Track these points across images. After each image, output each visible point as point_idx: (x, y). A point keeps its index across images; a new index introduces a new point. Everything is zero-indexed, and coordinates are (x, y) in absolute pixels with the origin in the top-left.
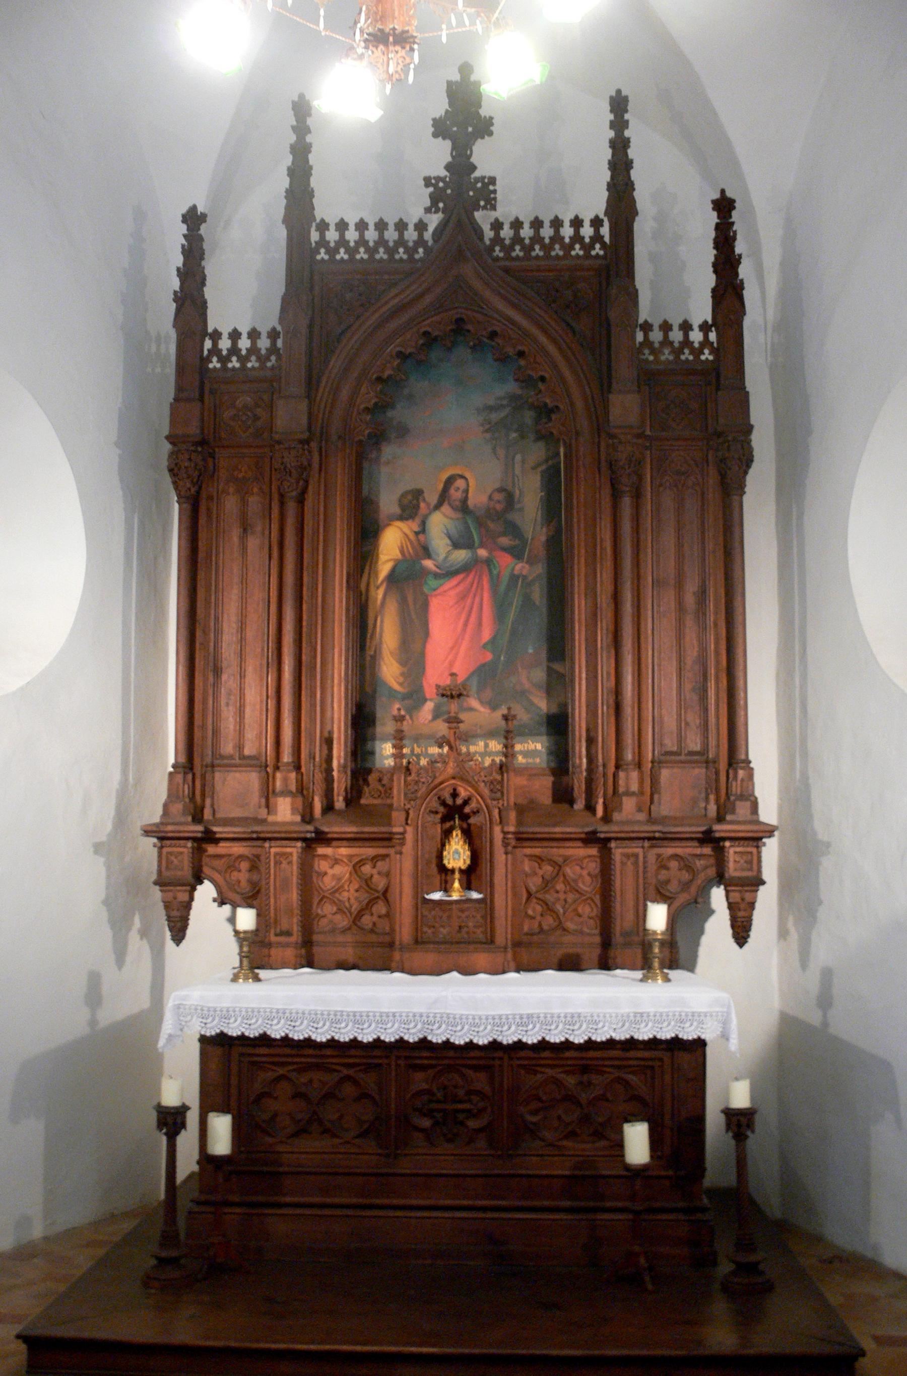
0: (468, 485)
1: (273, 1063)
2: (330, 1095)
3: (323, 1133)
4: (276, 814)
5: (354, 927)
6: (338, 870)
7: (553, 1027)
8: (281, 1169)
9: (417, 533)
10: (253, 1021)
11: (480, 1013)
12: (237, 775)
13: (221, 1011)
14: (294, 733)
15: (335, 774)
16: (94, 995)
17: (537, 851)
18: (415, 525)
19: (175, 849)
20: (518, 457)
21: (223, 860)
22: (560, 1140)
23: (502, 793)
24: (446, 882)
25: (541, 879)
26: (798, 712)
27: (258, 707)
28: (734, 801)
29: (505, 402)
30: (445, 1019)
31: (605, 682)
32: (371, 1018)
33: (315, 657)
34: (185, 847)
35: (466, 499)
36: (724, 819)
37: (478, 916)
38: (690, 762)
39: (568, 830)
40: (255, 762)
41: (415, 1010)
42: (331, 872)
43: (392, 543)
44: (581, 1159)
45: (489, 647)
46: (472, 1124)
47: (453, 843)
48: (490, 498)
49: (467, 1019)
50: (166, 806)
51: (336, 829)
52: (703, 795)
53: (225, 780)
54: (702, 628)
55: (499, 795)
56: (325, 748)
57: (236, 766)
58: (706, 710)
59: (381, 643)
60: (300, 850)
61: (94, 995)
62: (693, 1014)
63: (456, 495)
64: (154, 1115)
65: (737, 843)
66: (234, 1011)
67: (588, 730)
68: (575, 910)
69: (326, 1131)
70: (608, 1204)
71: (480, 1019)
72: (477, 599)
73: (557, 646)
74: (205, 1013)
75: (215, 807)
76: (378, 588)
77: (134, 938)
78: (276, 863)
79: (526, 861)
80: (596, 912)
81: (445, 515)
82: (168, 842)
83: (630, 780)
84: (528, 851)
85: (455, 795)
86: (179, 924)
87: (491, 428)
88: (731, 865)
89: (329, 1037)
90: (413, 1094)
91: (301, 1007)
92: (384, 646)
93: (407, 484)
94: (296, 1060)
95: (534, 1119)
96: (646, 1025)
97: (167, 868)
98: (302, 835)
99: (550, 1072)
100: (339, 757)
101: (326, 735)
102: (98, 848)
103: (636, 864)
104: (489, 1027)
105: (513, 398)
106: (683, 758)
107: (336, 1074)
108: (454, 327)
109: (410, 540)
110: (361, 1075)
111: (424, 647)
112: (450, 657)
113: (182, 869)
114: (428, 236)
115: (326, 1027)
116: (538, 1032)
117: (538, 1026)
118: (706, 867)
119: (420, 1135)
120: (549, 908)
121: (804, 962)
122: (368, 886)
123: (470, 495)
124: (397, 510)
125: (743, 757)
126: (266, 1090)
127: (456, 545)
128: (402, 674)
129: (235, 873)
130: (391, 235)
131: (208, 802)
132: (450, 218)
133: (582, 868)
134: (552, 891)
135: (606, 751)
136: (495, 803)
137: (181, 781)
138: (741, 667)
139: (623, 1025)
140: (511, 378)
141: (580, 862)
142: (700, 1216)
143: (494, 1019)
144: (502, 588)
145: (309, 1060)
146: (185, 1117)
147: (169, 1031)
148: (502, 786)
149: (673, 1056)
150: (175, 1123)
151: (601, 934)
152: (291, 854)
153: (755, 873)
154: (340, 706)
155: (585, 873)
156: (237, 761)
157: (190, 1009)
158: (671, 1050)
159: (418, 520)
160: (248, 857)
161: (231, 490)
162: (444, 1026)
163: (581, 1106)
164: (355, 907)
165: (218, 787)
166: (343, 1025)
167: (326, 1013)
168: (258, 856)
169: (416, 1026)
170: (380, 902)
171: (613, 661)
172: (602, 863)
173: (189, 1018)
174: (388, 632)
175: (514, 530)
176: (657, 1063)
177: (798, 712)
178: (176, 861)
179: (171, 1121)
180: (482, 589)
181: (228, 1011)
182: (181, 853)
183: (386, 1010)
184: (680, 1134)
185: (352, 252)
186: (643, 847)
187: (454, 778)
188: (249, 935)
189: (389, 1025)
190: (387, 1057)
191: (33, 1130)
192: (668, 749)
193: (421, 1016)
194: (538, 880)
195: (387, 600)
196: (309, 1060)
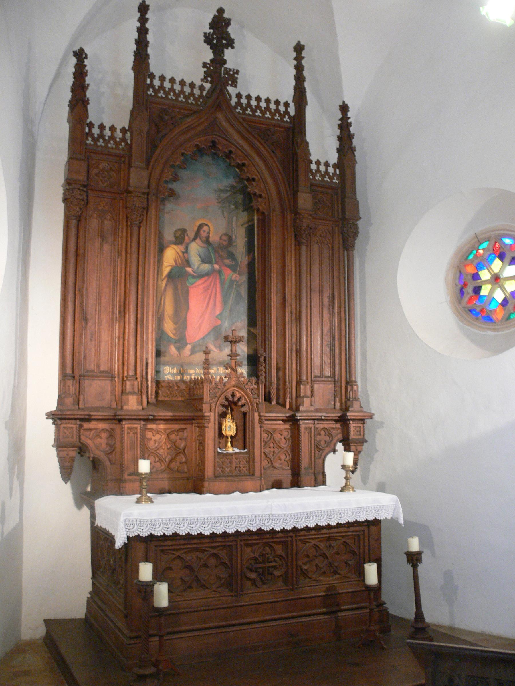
0: (210, 230)
1: (174, 550)
4: (128, 405)
6: (157, 437)
7: (322, 518)
8: (180, 611)
9: (183, 253)
10: (170, 526)
12: (99, 382)
18: (182, 248)
20: (234, 218)
21: (93, 432)
28: (352, 401)
29: (228, 189)
32: (302, 516)
34: (76, 424)
35: (208, 237)
36: (299, 410)
40: (107, 375)
41: (256, 513)
43: (170, 255)
44: (328, 586)
45: (219, 317)
46: (276, 573)
48: (221, 238)
51: (161, 414)
52: (333, 398)
54: (332, 314)
57: (96, 376)
58: (334, 356)
59: (163, 311)
62: (383, 506)
63: (204, 234)
66: (158, 521)
67: (277, 364)
68: (279, 457)
71: (288, 516)
72: (214, 291)
81: (197, 244)
85: (233, 396)
87: (221, 201)
89: (211, 532)
91: (195, 516)
92: (166, 313)
93: (178, 225)
94: (187, 546)
95: (305, 567)
99: (313, 542)
105: (232, 187)
107: (206, 553)
108: (211, 145)
109: (180, 256)
110: (221, 552)
111: (187, 314)
112: (200, 322)
113: (72, 437)
114: (204, 93)
115: (210, 526)
123: (211, 235)
124: (174, 239)
127: (203, 261)
128: (175, 329)
129: (99, 440)
130: (177, 87)
132: (215, 88)
135: (291, 377)
136: (255, 400)
138: (353, 335)
140: (231, 177)
145: (193, 546)
151: (291, 469)
152: (137, 428)
159: (184, 246)
160: (108, 430)
161: (95, 215)
163: (327, 558)
166: (219, 524)
167: (209, 518)
168: (113, 430)
170: (181, 454)
172: (343, 433)
175: (231, 256)
181: (155, 521)
182: (72, 428)
183: (241, 514)
185: (167, 93)
187: (234, 387)
188: (147, 476)
189: (243, 523)
193: (259, 516)
196: (193, 546)
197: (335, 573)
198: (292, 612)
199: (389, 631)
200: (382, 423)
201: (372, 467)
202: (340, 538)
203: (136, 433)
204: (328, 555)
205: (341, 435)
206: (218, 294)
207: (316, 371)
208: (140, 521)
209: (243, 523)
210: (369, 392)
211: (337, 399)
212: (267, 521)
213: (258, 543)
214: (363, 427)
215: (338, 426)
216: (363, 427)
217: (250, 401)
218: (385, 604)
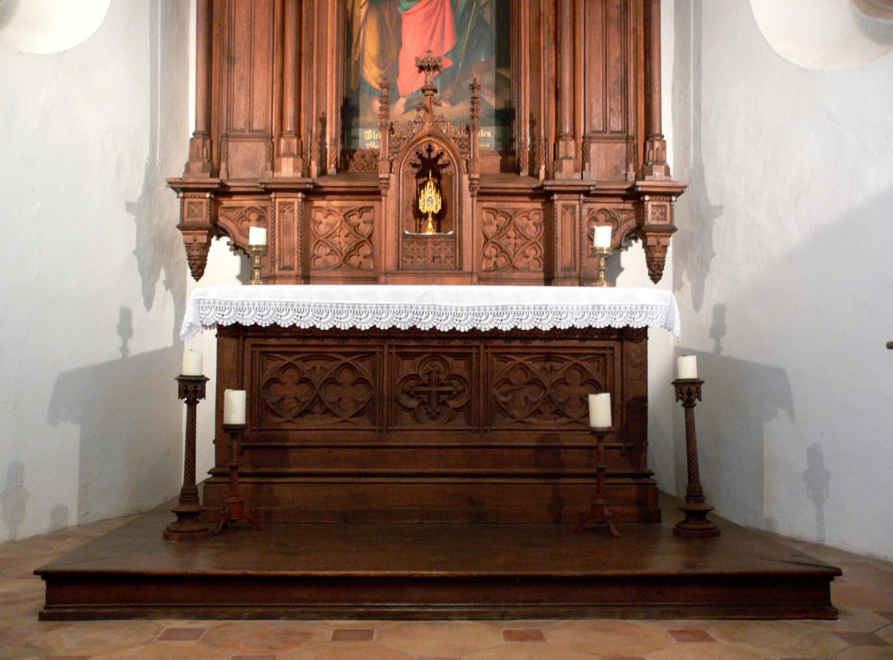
2: (331, 381)
3: (324, 413)
4: (280, 170)
5: (344, 264)
6: (331, 219)
8: (288, 444)
11: (462, 305)
12: (248, 144)
13: (237, 304)
14: (295, 113)
15: (328, 147)
16: (125, 327)
17: (493, 205)
19: (195, 200)
22: (528, 417)
23: (469, 149)
24: (420, 226)
25: (495, 227)
26: (692, 111)
27: (265, 91)
30: (432, 310)
31: (546, 73)
33: (312, 50)
34: (205, 198)
37: (449, 249)
38: (611, 138)
39: (520, 186)
40: (262, 134)
42: (325, 221)
45: (450, 56)
46: (453, 404)
47: (427, 192)
49: (451, 309)
50: (187, 166)
52: (624, 164)
53: (237, 148)
54: (625, 32)
55: (466, 150)
56: (320, 124)
58: (626, 97)
60: (300, 200)
61: (125, 327)
64: (176, 385)
65: (654, 198)
66: (248, 304)
67: (531, 115)
69: (327, 411)
70: (569, 471)
72: (441, 18)
73: (505, 55)
74: (221, 308)
75: (229, 170)
76: (361, 7)
77: (160, 286)
78: (280, 211)
79: (484, 212)
80: (541, 252)
82: (189, 194)
83: (569, 148)
84: (486, 204)
85: (430, 150)
86: (198, 262)
88: (649, 215)
90: (404, 378)
92: (366, 54)
95: (503, 399)
96: (603, 316)
97: (188, 216)
98: (302, 186)
99: (519, 360)
100: (331, 134)
101: (321, 115)
102: (129, 207)
103: (573, 213)
104: (470, 317)
106: (608, 135)
113: (201, 216)
115: (329, 318)
116: (511, 321)
117: (511, 316)
118: (627, 220)
119: (408, 414)
120: (502, 250)
121: (697, 306)
122: (355, 230)
125: (657, 132)
126: (274, 376)
128: (380, 76)
131: (223, 165)
133: (529, 219)
134: (505, 237)
135: (547, 130)
136: (463, 156)
137: (200, 145)
139: (583, 316)
141: (527, 214)
142: (645, 480)
143: (473, 310)
144: (461, 8)
146: (204, 387)
147: (190, 320)
148: (469, 143)
149: (622, 345)
150: (195, 392)
151: (544, 272)
152: (293, 203)
153: (668, 222)
154: (332, 94)
155: (531, 223)
156: (248, 133)
157: (209, 303)
158: (620, 340)
160: (256, 209)
162: (431, 316)
163: (545, 389)
164: (345, 248)
165: (231, 154)
166: (344, 315)
168: (265, 208)
169: (406, 316)
171: (554, 55)
173: (208, 310)
174: (369, 43)
176: (608, 352)
177: (692, 111)
178: (196, 210)
179: (192, 388)
180: (444, 11)
181: (243, 304)
184: (632, 409)
186: (579, 200)
187: (429, 136)
189: (384, 315)
190: (381, 346)
191: (70, 433)
192: (596, 129)
194: (493, 228)
195: (369, 16)
197: (559, 413)
198: (476, 467)
199: (659, 521)
200: (721, 207)
201: (707, 282)
202: (568, 357)
203: (293, 211)
204: (546, 385)
205: (634, 220)
206: (447, 22)
207: (595, 121)
208: (220, 303)
209: (384, 315)
210: (704, 162)
211: (631, 166)
212: (425, 315)
213: (420, 354)
214: (671, 206)
215: (629, 206)
216: (671, 206)
217: (456, 157)
218: (653, 474)
